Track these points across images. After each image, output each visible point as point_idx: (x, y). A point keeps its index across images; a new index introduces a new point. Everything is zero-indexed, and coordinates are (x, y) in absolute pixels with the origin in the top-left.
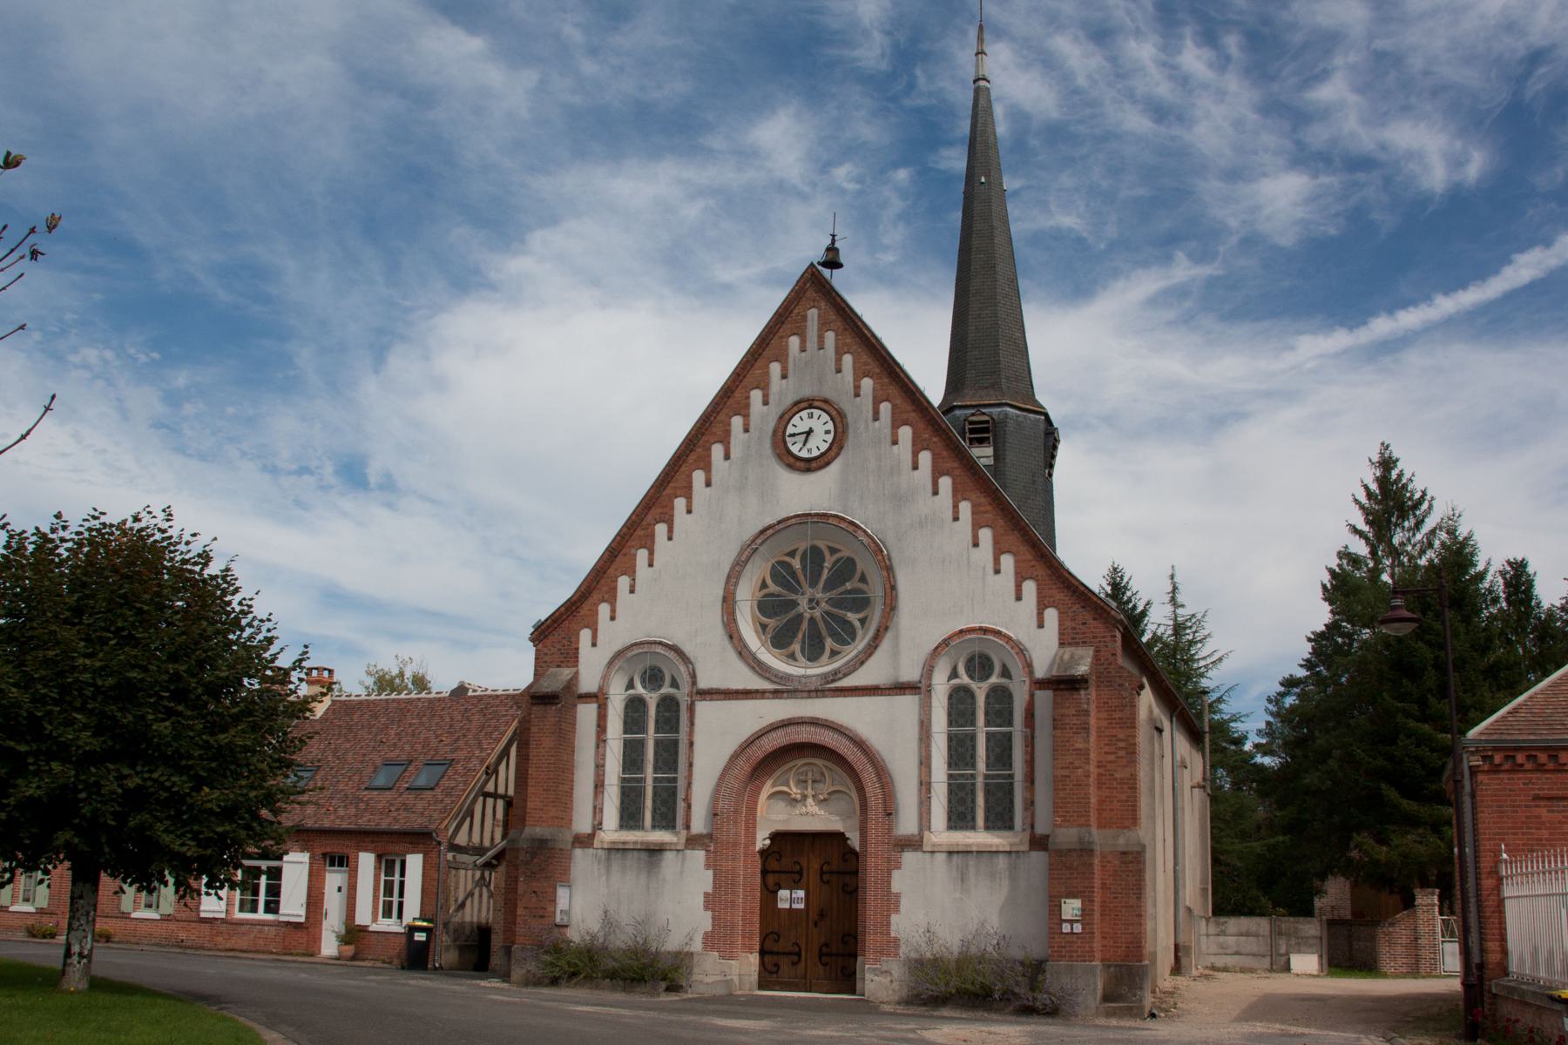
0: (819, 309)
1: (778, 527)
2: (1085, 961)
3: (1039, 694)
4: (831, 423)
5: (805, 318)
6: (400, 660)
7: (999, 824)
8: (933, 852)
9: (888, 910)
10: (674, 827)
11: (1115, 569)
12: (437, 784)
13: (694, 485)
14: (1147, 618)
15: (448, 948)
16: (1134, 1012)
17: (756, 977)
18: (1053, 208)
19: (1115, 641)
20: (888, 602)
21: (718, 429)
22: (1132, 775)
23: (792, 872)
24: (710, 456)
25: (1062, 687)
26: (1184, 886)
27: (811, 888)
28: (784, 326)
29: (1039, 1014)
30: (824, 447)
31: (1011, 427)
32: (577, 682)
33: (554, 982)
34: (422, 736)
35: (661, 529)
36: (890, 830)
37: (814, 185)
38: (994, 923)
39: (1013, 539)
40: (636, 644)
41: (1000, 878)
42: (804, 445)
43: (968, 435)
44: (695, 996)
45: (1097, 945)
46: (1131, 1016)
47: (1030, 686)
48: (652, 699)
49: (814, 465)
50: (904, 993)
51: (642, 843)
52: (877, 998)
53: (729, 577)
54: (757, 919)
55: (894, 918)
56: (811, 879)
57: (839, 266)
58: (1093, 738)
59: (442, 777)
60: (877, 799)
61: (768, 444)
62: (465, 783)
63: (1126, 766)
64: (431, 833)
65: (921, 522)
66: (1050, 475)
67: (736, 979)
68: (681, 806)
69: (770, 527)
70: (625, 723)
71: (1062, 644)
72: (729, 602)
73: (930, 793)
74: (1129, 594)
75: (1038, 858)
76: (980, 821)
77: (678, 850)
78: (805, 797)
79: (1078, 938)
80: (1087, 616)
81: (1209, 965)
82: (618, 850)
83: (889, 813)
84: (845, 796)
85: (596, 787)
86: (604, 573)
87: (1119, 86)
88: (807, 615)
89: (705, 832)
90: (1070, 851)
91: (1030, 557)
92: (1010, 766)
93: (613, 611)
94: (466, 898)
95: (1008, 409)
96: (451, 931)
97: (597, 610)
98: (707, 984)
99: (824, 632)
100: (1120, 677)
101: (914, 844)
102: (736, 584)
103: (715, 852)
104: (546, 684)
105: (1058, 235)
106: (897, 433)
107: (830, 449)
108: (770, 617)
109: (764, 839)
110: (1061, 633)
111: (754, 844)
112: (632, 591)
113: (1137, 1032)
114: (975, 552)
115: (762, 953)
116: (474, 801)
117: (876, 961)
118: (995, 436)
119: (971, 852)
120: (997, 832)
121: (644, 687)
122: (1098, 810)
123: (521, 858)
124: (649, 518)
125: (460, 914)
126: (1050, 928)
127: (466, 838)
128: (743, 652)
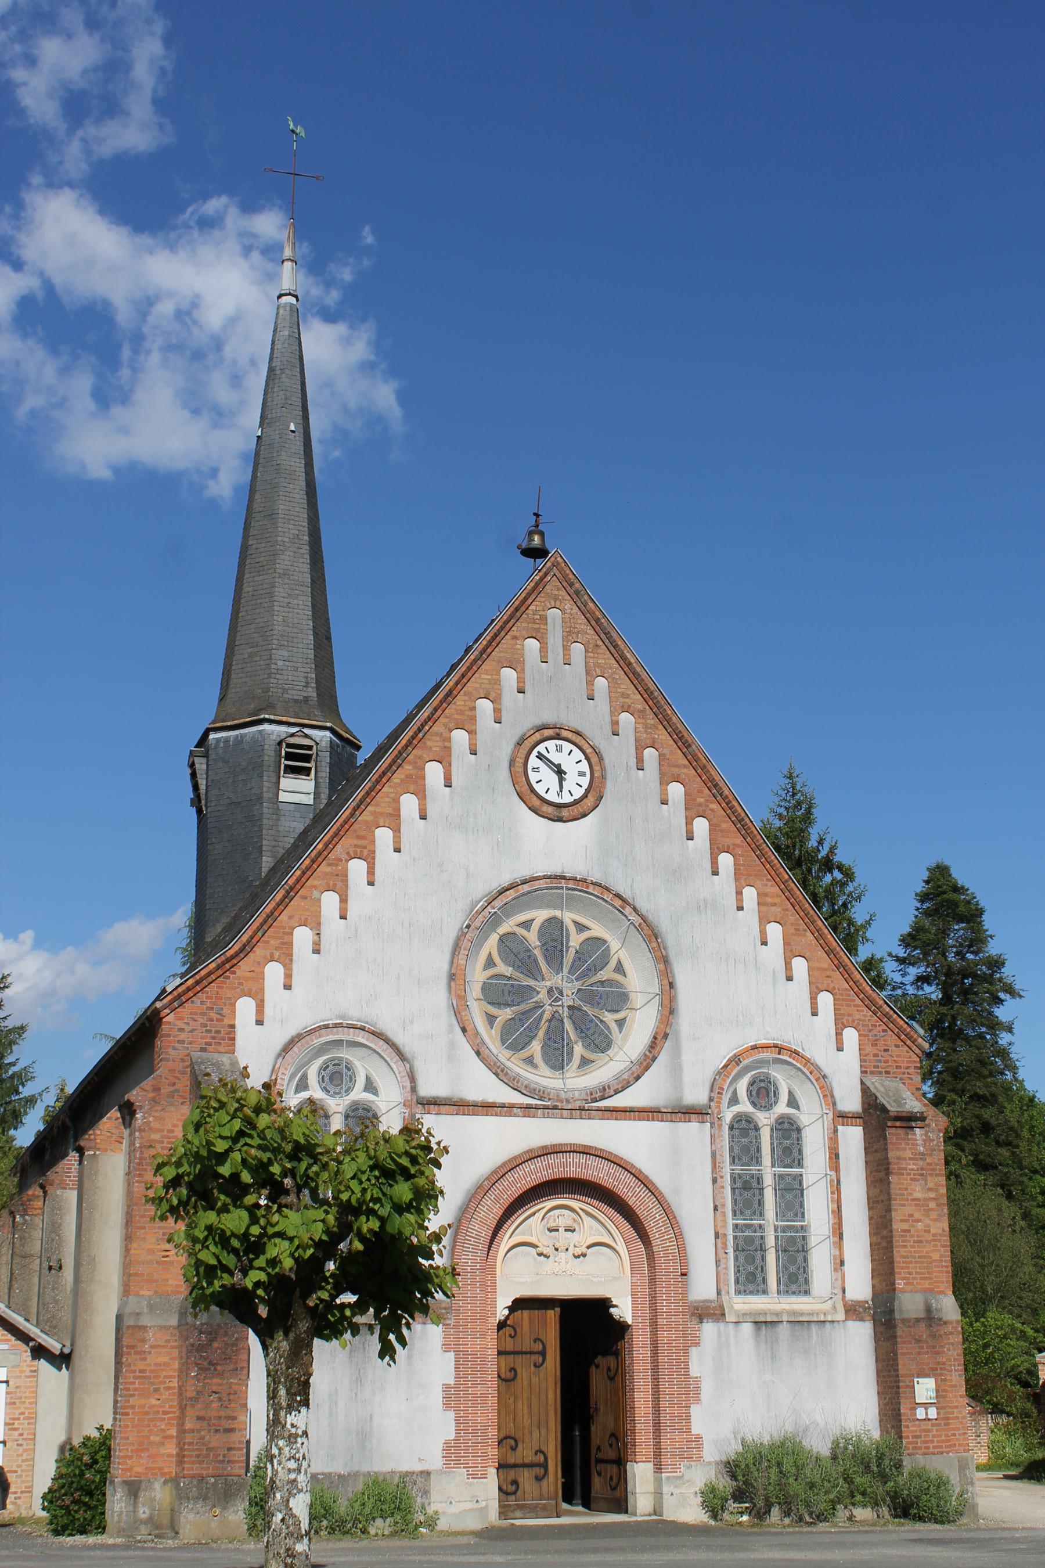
0: (563, 611)
4: (585, 762)
5: (544, 619)
20: (667, 1002)
21: (433, 743)
23: (531, 1353)
24: (423, 778)
25: (898, 1124)
36: (685, 1294)
43: (283, 760)
49: (565, 813)
107: (585, 796)
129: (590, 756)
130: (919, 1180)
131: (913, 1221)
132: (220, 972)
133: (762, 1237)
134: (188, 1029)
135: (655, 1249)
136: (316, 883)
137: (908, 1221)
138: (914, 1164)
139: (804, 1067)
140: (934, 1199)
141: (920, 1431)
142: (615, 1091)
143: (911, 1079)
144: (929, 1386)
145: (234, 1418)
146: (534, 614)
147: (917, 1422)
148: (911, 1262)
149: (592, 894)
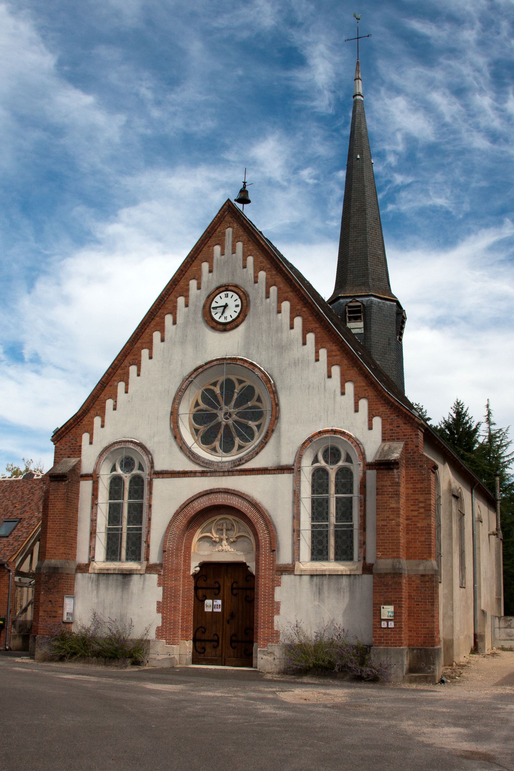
0: (233, 228)
1: (205, 367)
2: (396, 646)
3: (369, 472)
5: (224, 234)
6: (26, 461)
7: (344, 557)
8: (301, 575)
9: (273, 613)
10: (139, 559)
11: (458, 403)
12: (11, 534)
13: (154, 341)
14: (478, 433)
15: (15, 637)
16: (430, 679)
17: (191, 656)
18: (431, 194)
19: (418, 438)
20: (274, 414)
21: (169, 306)
22: (428, 524)
23: (214, 588)
24: (164, 322)
25: (382, 467)
26: (480, 597)
27: (225, 598)
28: (211, 239)
29: (366, 681)
30: (235, 315)
31: (374, 309)
32: (80, 467)
33: (62, 659)
34: (4, 504)
35: (133, 369)
36: (274, 561)
37: (289, 181)
38: (340, 621)
39: (353, 372)
40: (115, 443)
41: (344, 592)
42: (222, 314)
43: (347, 314)
44: (150, 668)
45: (405, 635)
46: (427, 682)
47: (364, 467)
48: (127, 478)
49: (228, 327)
50: (282, 667)
51: (119, 570)
52: (265, 670)
53: (175, 399)
54: (191, 618)
55: (276, 618)
56: (225, 593)
57: (248, 202)
58: (402, 501)
59: (14, 529)
60: (266, 541)
61: (200, 315)
62: (28, 533)
63: (424, 519)
64: (4, 564)
65: (295, 363)
66: (401, 340)
67: (177, 657)
68: (144, 545)
69: (201, 367)
70: (110, 493)
71: (384, 440)
72: (174, 415)
73: (299, 537)
74: (467, 418)
75: (368, 579)
76: (332, 554)
77: (141, 574)
78: (221, 540)
79: (391, 631)
80: (400, 422)
81: (500, 647)
82: (104, 574)
83: (274, 549)
84: (246, 539)
85: (91, 533)
86: (98, 397)
87: (470, 122)
88: (224, 423)
89: (158, 562)
90: (386, 574)
91: (364, 384)
92: (351, 519)
93: (103, 422)
94: (28, 605)
95: (373, 298)
96: (17, 626)
97: (93, 421)
98: (159, 660)
99: (234, 434)
100: (421, 461)
101: (289, 570)
102: (179, 403)
103: (163, 575)
104: (59, 468)
105: (435, 210)
106: (281, 305)
107: (238, 316)
108: (200, 425)
109: (196, 567)
110: (384, 434)
111: (189, 570)
112: (115, 409)
113: (424, 694)
114: (329, 382)
115: (195, 640)
116: (34, 544)
117: (265, 646)
118: (365, 315)
119: (325, 575)
120: (342, 563)
121: (122, 470)
122: (406, 547)
123: (42, 579)
124: (126, 362)
125: (24, 615)
126: (374, 625)
127: (28, 568)
128: (183, 447)
129: (241, 296)
130: (394, 497)
131: (389, 520)
132: (76, 423)
133: (327, 531)
134: (63, 448)
135: (260, 538)
136: (116, 378)
137: (386, 520)
138: (392, 489)
139: (349, 440)
140: (423, 507)
141: (384, 634)
142: (246, 461)
143: (412, 441)
144: (389, 610)
145: (57, 612)
146: (219, 233)
147: (382, 629)
148: (386, 543)
149: (239, 365)
